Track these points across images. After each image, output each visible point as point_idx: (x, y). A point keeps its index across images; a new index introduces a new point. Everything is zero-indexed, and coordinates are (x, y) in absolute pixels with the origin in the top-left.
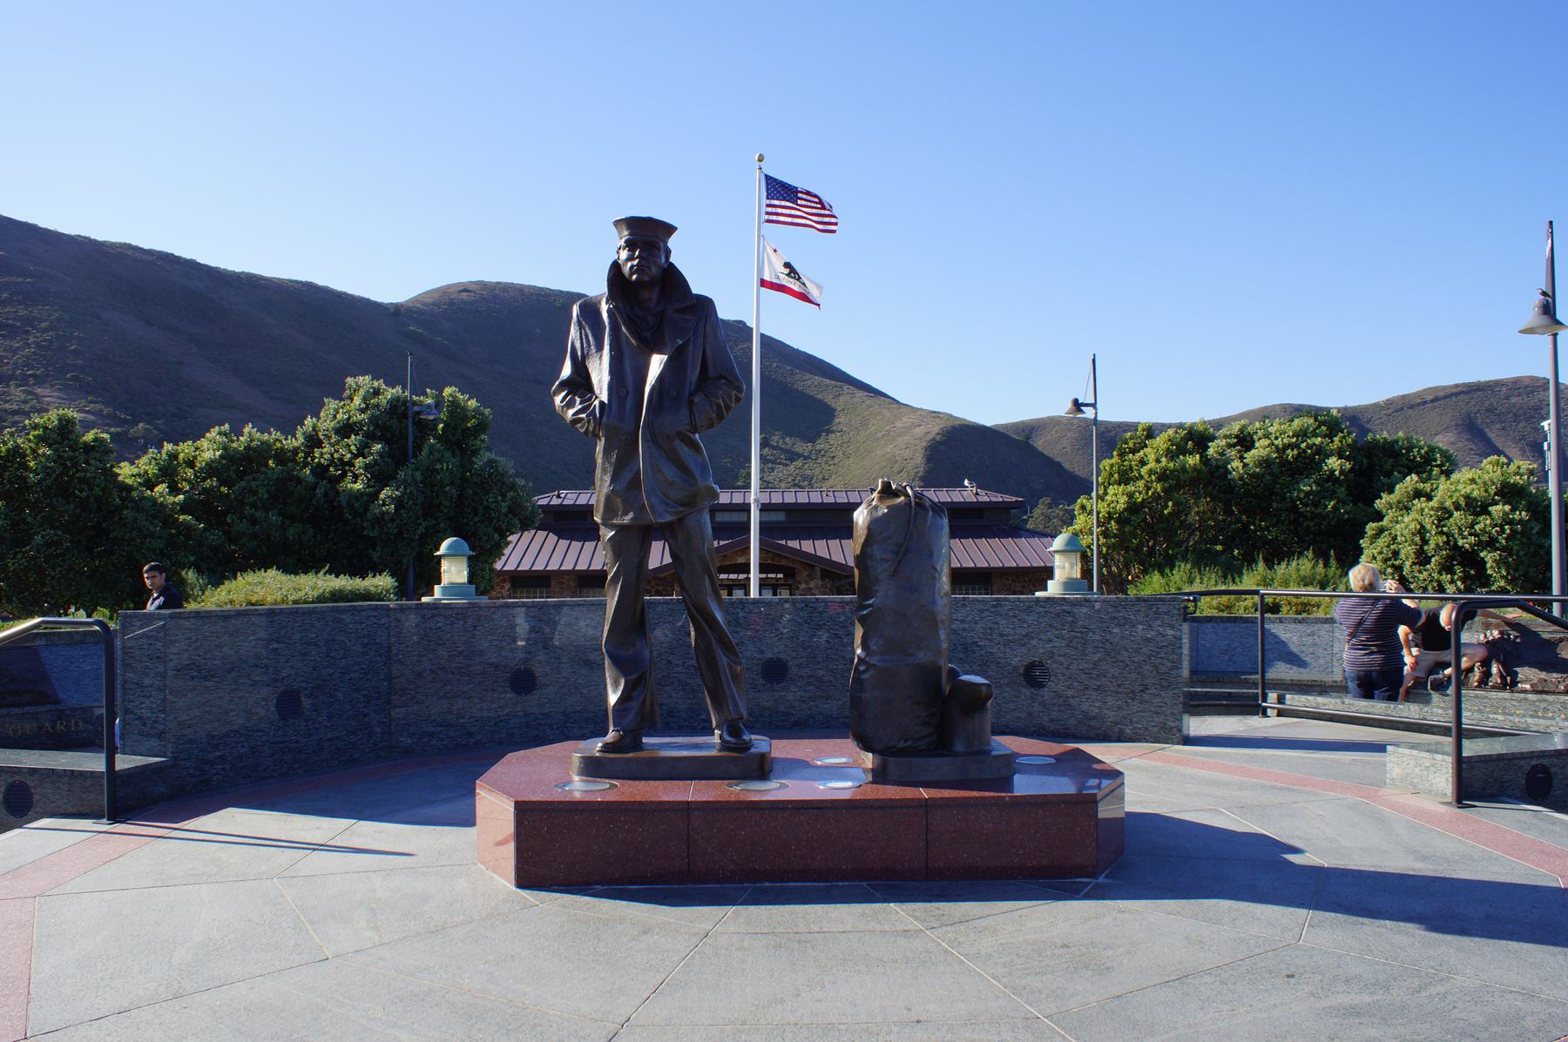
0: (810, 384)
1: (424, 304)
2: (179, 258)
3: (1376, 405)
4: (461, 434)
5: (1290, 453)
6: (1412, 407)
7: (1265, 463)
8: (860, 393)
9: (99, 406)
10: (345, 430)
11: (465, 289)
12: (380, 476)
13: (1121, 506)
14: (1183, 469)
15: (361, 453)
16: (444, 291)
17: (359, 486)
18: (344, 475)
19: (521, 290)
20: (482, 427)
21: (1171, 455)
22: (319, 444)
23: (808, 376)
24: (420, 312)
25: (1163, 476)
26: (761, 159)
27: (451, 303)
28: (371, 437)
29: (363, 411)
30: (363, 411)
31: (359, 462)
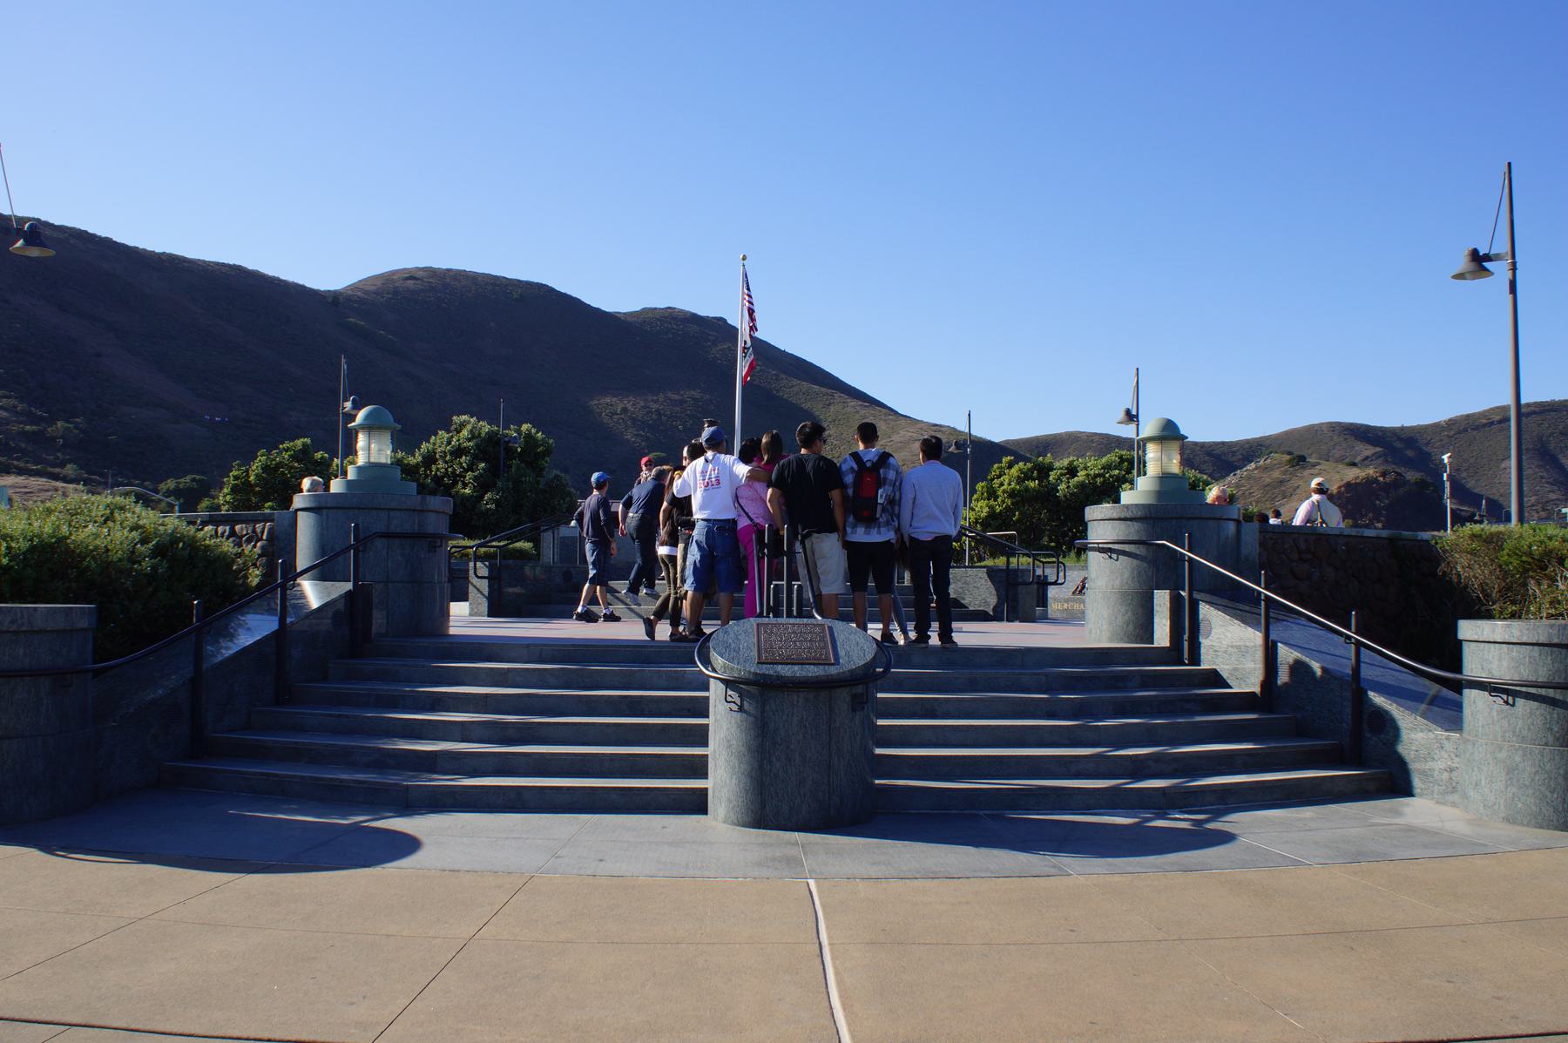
0: (796, 391)
1: (366, 292)
2: (94, 236)
3: (1436, 426)
4: (532, 454)
5: (1099, 480)
6: (1477, 428)
7: (1082, 485)
8: (853, 403)
9: (13, 402)
10: (459, 452)
11: (411, 275)
12: (483, 485)
13: (984, 515)
14: (1027, 489)
15: (470, 468)
16: (388, 278)
17: (467, 491)
18: (455, 483)
19: (474, 278)
20: (548, 452)
21: (1020, 480)
22: (435, 461)
23: (795, 382)
24: (361, 301)
25: (1012, 494)
26: (744, 258)
27: (396, 292)
28: (476, 458)
29: (469, 440)
30: (469, 440)
31: (469, 475)
